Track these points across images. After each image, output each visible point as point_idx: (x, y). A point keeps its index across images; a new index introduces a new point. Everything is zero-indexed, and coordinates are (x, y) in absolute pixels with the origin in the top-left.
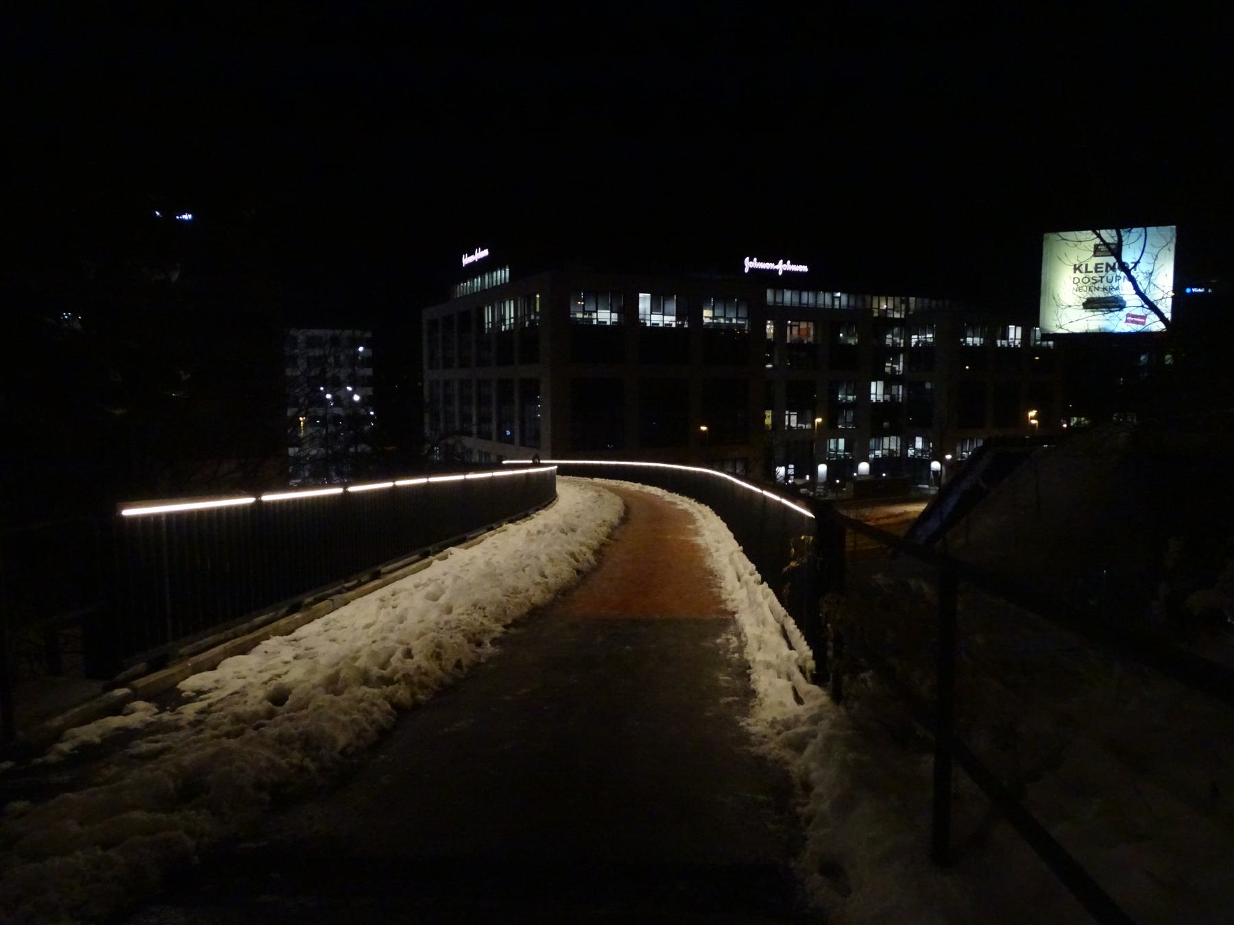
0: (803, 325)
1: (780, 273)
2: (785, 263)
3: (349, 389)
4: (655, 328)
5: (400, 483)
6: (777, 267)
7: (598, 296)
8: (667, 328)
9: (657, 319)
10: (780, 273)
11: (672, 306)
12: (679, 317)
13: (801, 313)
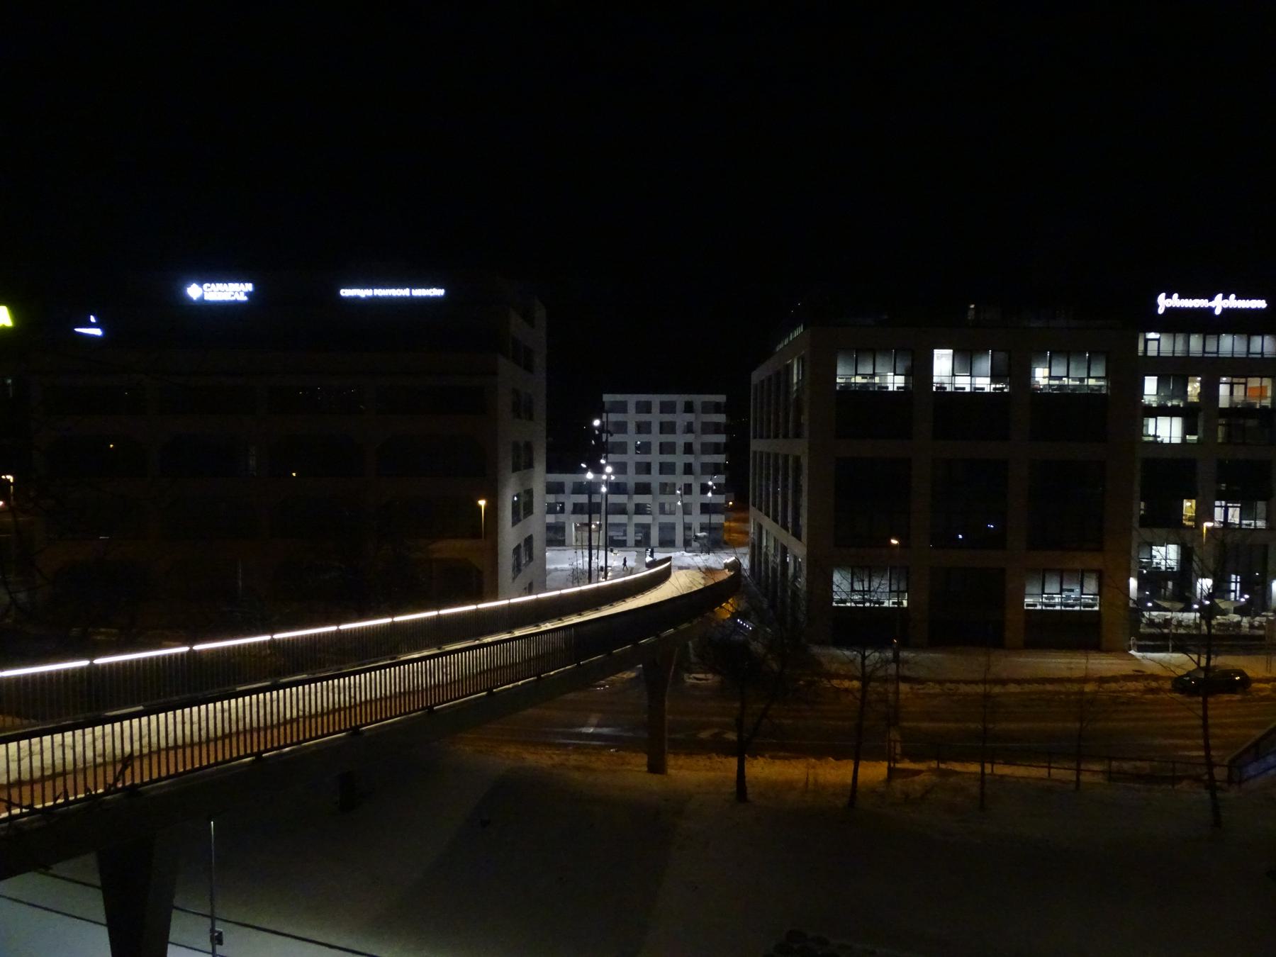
0: (1254, 382)
1: (1218, 312)
2: (1226, 297)
3: (584, 466)
4: (958, 395)
5: (443, 612)
6: (1212, 304)
7: (868, 349)
8: (976, 395)
9: (963, 382)
10: (1218, 312)
11: (985, 364)
12: (995, 378)
13: (1241, 368)
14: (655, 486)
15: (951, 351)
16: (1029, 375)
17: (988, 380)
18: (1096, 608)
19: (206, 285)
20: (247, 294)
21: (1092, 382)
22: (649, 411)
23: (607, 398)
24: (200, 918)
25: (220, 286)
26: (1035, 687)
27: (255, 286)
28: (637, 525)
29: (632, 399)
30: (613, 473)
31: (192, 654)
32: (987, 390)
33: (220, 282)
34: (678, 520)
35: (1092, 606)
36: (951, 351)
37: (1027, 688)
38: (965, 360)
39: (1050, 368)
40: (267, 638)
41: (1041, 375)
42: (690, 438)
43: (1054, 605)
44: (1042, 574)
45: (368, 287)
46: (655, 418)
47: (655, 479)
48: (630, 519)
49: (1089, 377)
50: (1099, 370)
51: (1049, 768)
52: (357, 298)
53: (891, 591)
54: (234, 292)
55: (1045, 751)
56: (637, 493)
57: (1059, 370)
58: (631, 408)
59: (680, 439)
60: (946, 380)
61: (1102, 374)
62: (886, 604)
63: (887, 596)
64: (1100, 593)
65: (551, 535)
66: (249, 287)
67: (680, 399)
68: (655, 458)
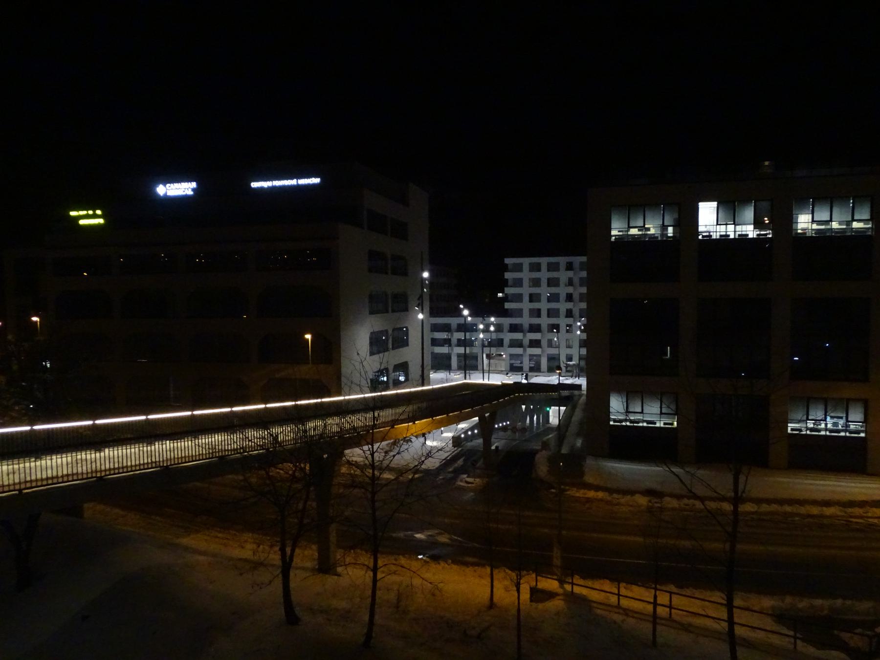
9: (731, 231)
11: (749, 213)
14: (544, 327)
15: (715, 204)
16: (791, 221)
17: (751, 227)
18: (863, 435)
19: (168, 185)
20: (193, 190)
21: (855, 225)
22: (539, 270)
23: (508, 261)
24: (719, 606)
25: (176, 185)
26: (774, 507)
27: (197, 184)
28: (530, 355)
29: (526, 262)
30: (470, 315)
31: (32, 431)
32: (751, 236)
33: (184, 182)
34: (563, 353)
35: (858, 432)
36: (715, 204)
37: (765, 508)
38: (730, 209)
39: (813, 214)
40: (90, 423)
41: (804, 222)
42: (570, 290)
43: (819, 431)
44: (807, 402)
45: (269, 180)
46: (544, 275)
47: (544, 321)
48: (525, 351)
49: (853, 220)
50: (864, 213)
51: (656, 589)
52: (262, 189)
53: (661, 413)
54: (183, 189)
55: (655, 571)
56: (529, 332)
57: (823, 215)
58: (526, 267)
59: (563, 291)
60: (711, 229)
61: (867, 216)
62: (658, 425)
63: (653, 415)
64: (866, 421)
65: (473, 362)
66: (194, 185)
67: (562, 260)
68: (544, 306)
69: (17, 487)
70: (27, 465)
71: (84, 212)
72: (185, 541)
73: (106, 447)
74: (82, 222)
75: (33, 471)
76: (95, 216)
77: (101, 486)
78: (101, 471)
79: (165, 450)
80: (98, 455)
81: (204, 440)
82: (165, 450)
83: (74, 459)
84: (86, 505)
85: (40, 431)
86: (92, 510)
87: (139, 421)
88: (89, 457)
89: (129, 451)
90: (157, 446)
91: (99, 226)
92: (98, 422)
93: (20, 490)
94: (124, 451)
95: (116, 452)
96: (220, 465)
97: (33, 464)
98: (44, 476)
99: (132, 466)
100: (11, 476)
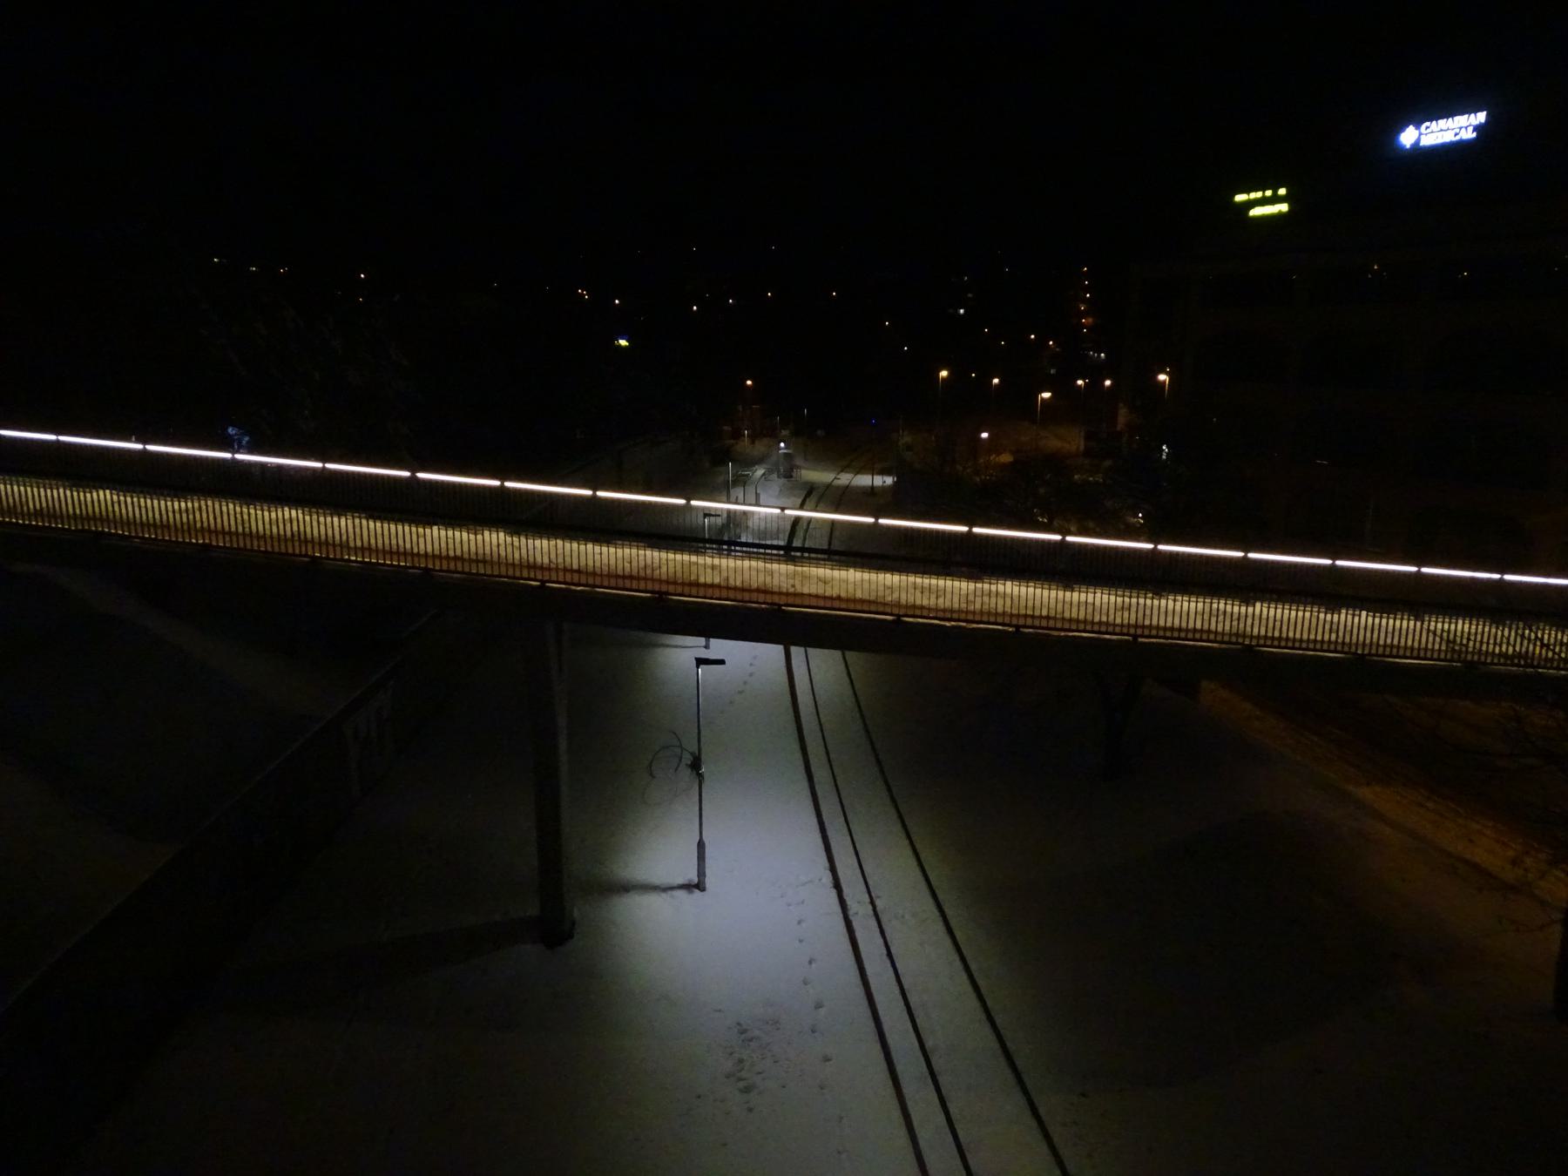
20: (1476, 128)
31: (1333, 566)
54: (1458, 128)
69: (1132, 631)
70: (1142, 601)
71: (1259, 195)
72: (1366, 793)
73: (1170, 592)
74: (1256, 212)
75: (1155, 612)
76: (1275, 200)
77: (1244, 662)
78: (1252, 637)
79: (1361, 625)
80: (1243, 609)
81: (1439, 625)
82: (1361, 625)
83: (1279, 616)
84: (1204, 684)
85: (1342, 568)
86: (1212, 693)
87: (1231, 559)
88: (1229, 608)
89: (1193, 605)
90: (1343, 616)
91: (1280, 216)
92: (1508, 577)
93: (1135, 637)
94: (1193, 605)
95: (1272, 611)
96: (1464, 676)
97: (1149, 602)
98: (1169, 624)
99: (1301, 640)
100: (1119, 614)
